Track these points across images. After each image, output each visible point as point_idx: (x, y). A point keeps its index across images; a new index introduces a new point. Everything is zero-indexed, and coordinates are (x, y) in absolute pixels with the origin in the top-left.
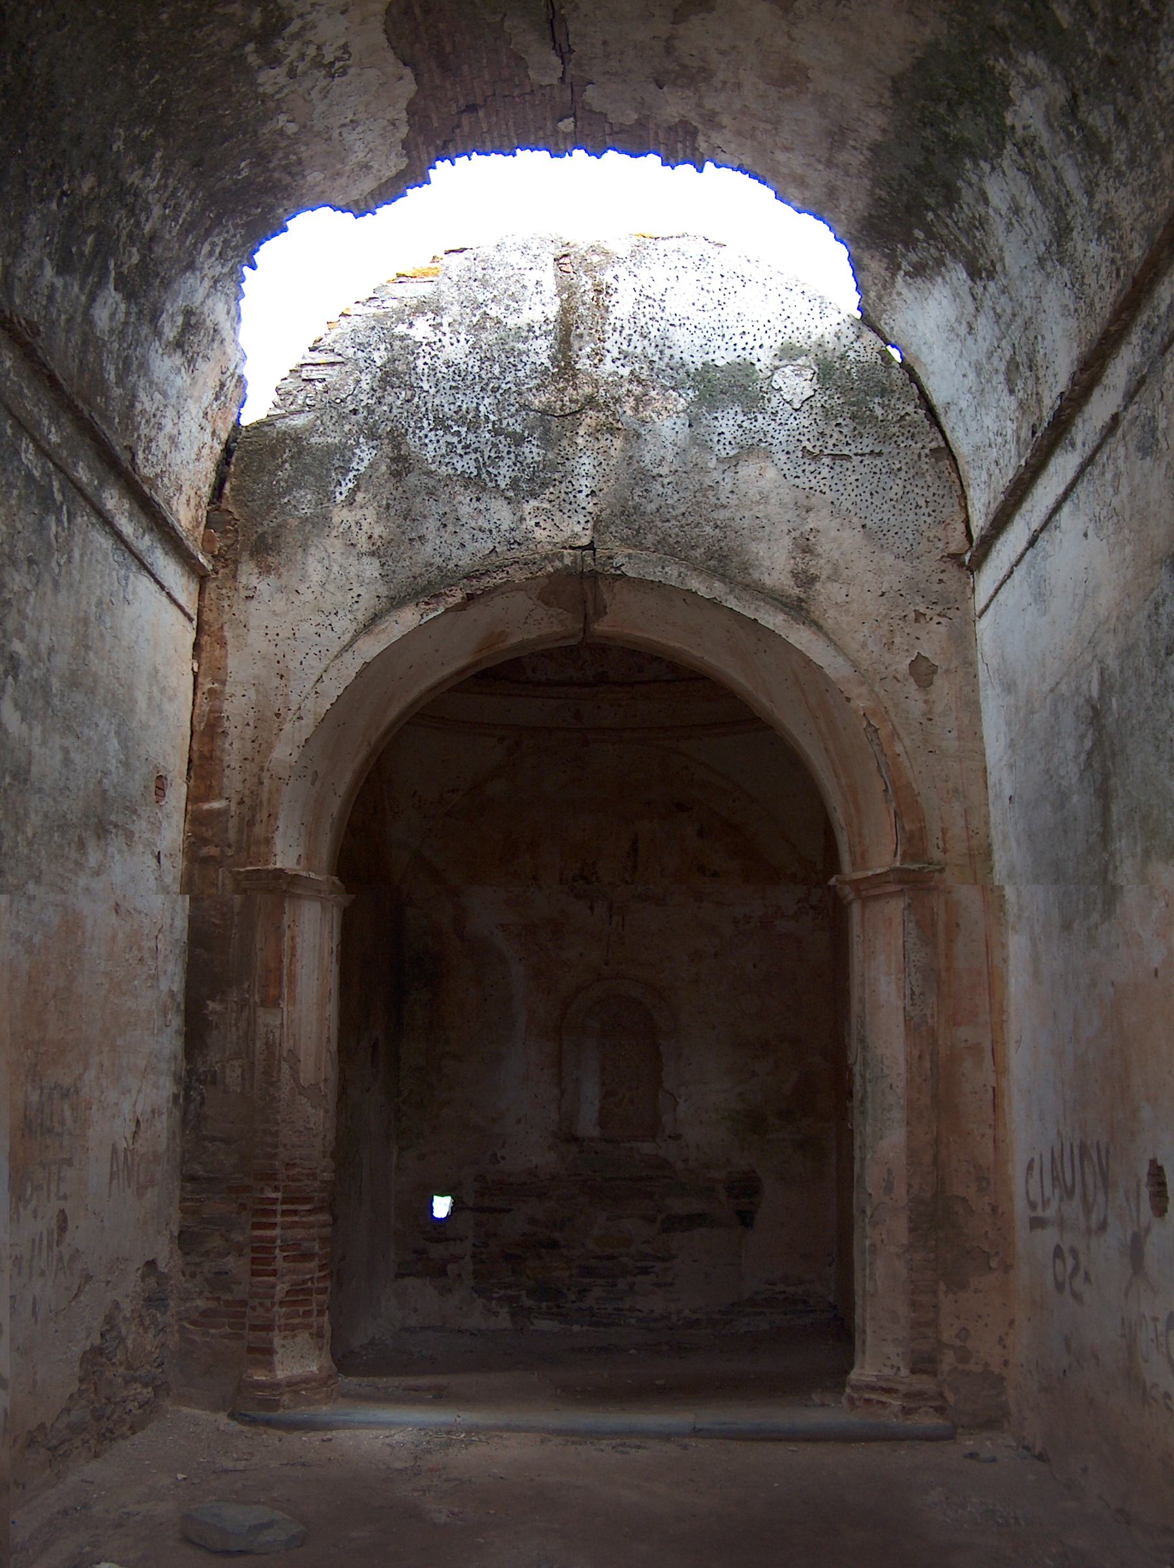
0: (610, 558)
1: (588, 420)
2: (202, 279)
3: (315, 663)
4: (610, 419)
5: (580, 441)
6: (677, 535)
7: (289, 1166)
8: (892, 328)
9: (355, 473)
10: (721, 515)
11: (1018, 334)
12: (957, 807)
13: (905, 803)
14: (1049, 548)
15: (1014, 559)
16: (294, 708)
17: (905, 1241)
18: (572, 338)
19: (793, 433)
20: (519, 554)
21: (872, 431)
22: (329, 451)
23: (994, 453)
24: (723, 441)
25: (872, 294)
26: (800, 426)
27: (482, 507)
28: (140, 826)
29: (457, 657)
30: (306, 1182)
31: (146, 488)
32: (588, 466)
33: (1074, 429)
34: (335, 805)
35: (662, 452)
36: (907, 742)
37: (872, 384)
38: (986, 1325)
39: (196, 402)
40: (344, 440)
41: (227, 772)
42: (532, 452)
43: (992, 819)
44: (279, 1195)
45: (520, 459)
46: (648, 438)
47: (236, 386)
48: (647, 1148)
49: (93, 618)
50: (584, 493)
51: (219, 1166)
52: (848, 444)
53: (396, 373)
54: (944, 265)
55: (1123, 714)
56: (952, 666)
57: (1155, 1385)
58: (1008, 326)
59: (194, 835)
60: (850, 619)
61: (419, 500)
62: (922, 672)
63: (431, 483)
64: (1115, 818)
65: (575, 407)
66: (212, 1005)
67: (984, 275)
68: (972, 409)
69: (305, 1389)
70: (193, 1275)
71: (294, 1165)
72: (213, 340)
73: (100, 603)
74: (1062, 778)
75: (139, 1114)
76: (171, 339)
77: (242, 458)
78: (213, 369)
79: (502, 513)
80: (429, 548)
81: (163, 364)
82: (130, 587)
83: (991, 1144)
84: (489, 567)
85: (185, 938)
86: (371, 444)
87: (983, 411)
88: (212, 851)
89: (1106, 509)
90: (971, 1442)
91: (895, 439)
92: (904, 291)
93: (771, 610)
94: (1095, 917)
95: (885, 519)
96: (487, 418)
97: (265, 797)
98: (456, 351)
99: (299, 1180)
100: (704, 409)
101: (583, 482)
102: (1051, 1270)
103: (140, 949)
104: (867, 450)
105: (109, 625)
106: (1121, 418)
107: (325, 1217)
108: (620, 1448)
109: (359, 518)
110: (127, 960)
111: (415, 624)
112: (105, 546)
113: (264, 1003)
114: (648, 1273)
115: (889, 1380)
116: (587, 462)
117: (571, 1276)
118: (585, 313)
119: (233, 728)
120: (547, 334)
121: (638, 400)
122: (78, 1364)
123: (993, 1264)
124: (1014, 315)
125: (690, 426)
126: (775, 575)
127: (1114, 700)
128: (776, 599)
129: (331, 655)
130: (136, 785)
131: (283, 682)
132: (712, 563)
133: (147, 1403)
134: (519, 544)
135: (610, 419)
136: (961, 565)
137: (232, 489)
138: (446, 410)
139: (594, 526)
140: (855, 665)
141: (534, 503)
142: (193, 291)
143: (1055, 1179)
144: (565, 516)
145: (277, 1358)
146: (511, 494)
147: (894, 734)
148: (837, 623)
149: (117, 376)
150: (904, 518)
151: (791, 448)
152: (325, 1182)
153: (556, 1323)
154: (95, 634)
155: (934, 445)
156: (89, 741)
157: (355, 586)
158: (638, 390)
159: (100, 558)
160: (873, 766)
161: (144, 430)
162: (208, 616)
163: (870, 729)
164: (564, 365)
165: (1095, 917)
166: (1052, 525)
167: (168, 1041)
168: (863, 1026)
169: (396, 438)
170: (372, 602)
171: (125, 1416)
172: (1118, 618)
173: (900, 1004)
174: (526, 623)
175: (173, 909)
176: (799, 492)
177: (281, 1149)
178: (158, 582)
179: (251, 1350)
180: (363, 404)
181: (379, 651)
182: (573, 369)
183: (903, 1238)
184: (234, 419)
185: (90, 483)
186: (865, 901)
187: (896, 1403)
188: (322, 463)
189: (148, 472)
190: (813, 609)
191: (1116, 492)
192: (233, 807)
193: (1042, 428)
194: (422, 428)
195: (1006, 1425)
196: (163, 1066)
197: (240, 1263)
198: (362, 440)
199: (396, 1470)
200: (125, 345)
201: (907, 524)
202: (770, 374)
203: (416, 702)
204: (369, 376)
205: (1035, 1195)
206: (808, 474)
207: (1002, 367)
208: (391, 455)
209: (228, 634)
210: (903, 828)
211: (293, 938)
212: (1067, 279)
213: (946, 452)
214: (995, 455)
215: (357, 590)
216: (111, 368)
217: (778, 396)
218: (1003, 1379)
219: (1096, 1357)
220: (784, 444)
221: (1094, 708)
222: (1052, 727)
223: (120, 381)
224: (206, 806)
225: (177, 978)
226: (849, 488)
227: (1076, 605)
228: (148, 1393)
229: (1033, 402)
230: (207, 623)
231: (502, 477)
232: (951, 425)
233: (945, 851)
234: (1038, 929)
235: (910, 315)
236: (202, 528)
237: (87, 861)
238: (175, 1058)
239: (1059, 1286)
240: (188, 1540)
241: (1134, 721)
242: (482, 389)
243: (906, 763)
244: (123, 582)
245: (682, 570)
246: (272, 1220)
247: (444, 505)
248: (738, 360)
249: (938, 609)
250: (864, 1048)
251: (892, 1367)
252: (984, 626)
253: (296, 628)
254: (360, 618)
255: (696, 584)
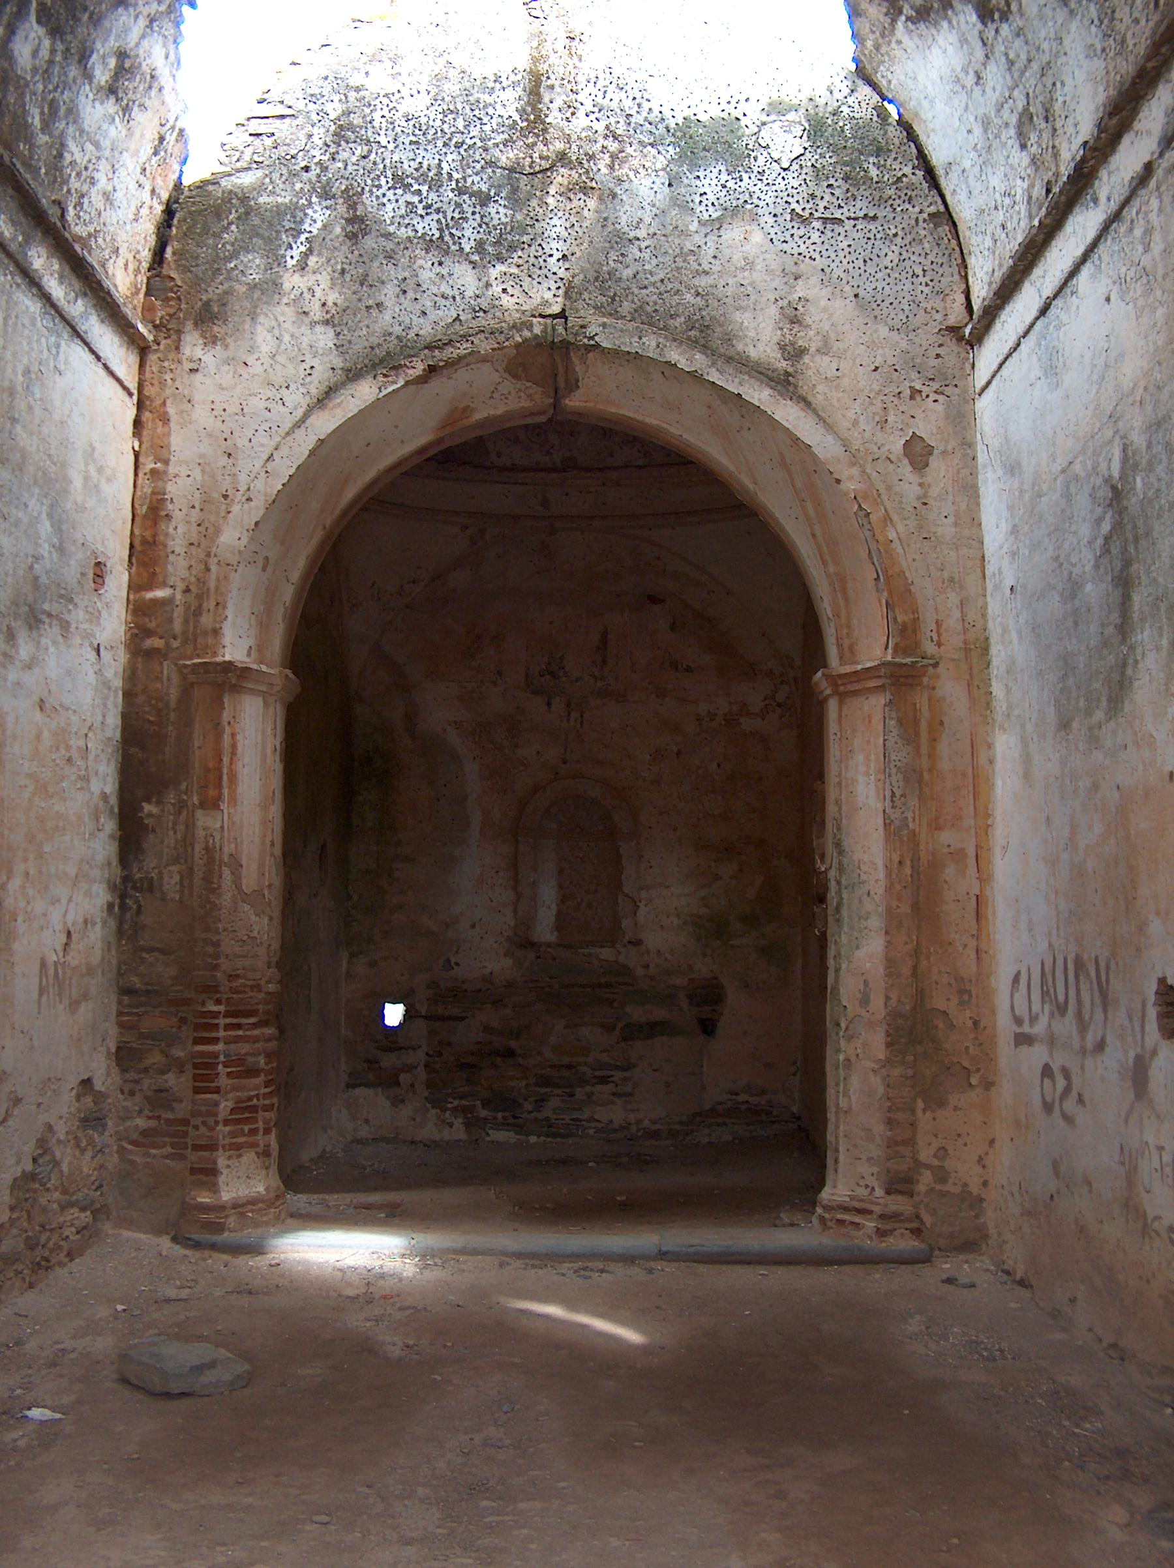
0: (582, 327)
1: (559, 179)
2: (137, 17)
3: (265, 441)
4: (584, 178)
5: (550, 200)
6: (655, 304)
7: (232, 977)
8: (890, 82)
9: (307, 235)
10: (703, 282)
11: (1033, 82)
12: (953, 598)
13: (897, 593)
14: (1064, 317)
15: (1021, 330)
16: (243, 488)
17: (882, 1057)
18: (542, 90)
19: (781, 194)
20: (484, 323)
21: (866, 194)
22: (279, 212)
23: (1000, 216)
24: (705, 202)
25: (869, 44)
26: (789, 187)
27: (445, 272)
28: (77, 616)
29: (416, 434)
30: (251, 994)
31: (77, 248)
32: (559, 227)
33: (1097, 183)
34: (287, 593)
35: (640, 213)
36: (901, 528)
37: (866, 143)
38: (965, 1145)
39: (132, 156)
40: (295, 200)
41: (171, 558)
42: (499, 213)
43: (990, 611)
44: (222, 1008)
45: (485, 220)
46: (624, 198)
47: (177, 141)
48: (606, 953)
49: (19, 388)
50: (555, 257)
51: (159, 975)
52: (840, 206)
53: (351, 127)
54: (951, 7)
55: (1150, 494)
56: (950, 448)
57: (1157, 1218)
58: (1022, 73)
59: (137, 626)
60: (841, 394)
61: (376, 264)
62: (918, 453)
63: (390, 246)
64: (1136, 608)
65: (545, 164)
66: (148, 808)
67: (996, 16)
68: (977, 169)
69: (252, 1211)
70: (132, 1093)
71: (237, 976)
72: (150, 87)
73: (27, 372)
74: (1074, 565)
75: (69, 925)
76: (103, 83)
77: (185, 220)
78: (151, 120)
79: (466, 278)
80: (387, 316)
81: (95, 112)
82: (62, 357)
83: (973, 956)
84: (454, 337)
85: (118, 735)
86: (324, 204)
87: (990, 170)
88: (157, 643)
89: (1133, 269)
90: (948, 1266)
91: (890, 202)
92: (905, 39)
93: (756, 385)
94: (1099, 715)
95: (879, 289)
96: (450, 175)
97: (212, 584)
98: (417, 105)
99: (245, 992)
100: (685, 168)
101: (554, 245)
102: (1039, 1089)
103: (68, 748)
104: (861, 214)
105: (38, 396)
106: (1155, 166)
107: (270, 1031)
108: (582, 1272)
109: (312, 284)
110: (54, 760)
111: (372, 398)
112: (32, 309)
113: (203, 805)
114: (607, 1083)
115: (862, 1200)
116: (558, 223)
117: (527, 1086)
118: (557, 62)
119: (177, 511)
120: (514, 85)
121: (614, 157)
122: (8, 1191)
123: (974, 1081)
124: (1029, 61)
125: (670, 185)
126: (761, 347)
127: (1138, 480)
128: (761, 373)
129: (282, 432)
130: (71, 573)
131: (231, 461)
132: (692, 333)
133: (85, 1228)
134: (485, 312)
135: (584, 178)
136: (961, 338)
137: (174, 253)
138: (406, 166)
139: (566, 293)
140: (846, 445)
141: (500, 268)
142: (126, 30)
143: (1044, 994)
144: (535, 282)
145: (222, 1179)
146: (476, 258)
147: (887, 518)
148: (827, 399)
149: (43, 121)
150: (899, 287)
151: (779, 211)
152: (271, 993)
153: (512, 1134)
154: (23, 406)
155: (932, 209)
156: (17, 523)
157: (308, 357)
158: (613, 146)
159: (26, 322)
160: (864, 553)
161: (74, 184)
162: (149, 391)
163: (862, 513)
164: (534, 120)
165: (1099, 715)
166: (1068, 290)
167: (99, 846)
168: (839, 829)
169: (352, 198)
170: (326, 375)
171: (62, 1243)
172: (1146, 389)
173: (880, 805)
174: (492, 397)
175: (105, 705)
176: (787, 258)
177: (222, 960)
178: (92, 352)
179: (193, 1171)
180: (316, 160)
181: (334, 427)
182: (543, 123)
183: (881, 1053)
184: (175, 176)
185: (14, 238)
186: (842, 697)
187: (870, 1225)
188: (271, 225)
189: (80, 230)
190: (800, 384)
191: (1147, 249)
192: (178, 596)
193: (1060, 183)
194: (379, 187)
195: (984, 1248)
196: (96, 873)
197: (182, 1079)
198: (314, 199)
199: (348, 1297)
200: (51, 87)
201: (901, 294)
202: (756, 130)
203: (373, 483)
204: (322, 130)
205: (1022, 1010)
206: (796, 238)
207: (1014, 120)
208: (346, 216)
209: (171, 410)
210: (895, 619)
211: (233, 735)
212: (1094, 15)
213: (946, 217)
214: (1001, 218)
215: (310, 362)
216: (35, 111)
217: (765, 153)
218: (981, 1200)
219: (1089, 1184)
220: (772, 206)
221: (1114, 488)
222: (1063, 511)
223: (46, 126)
224: (150, 595)
225: (110, 779)
226: (841, 254)
227: (1095, 377)
228: (86, 1217)
229: (1048, 157)
230: (148, 398)
231: (466, 239)
232: (952, 187)
233: (939, 645)
234: (1029, 728)
235: (910, 66)
236: (141, 296)
237: (17, 653)
238: (109, 864)
239: (1048, 1107)
240: (125, 1381)
241: (1163, 502)
242: (445, 145)
243: (899, 549)
244: (54, 351)
245: (661, 340)
246: (214, 1035)
247: (403, 270)
248: (722, 115)
249: (935, 385)
250: (840, 853)
251: (867, 1186)
252: (985, 405)
253: (244, 403)
254: (314, 391)
255: (675, 355)
